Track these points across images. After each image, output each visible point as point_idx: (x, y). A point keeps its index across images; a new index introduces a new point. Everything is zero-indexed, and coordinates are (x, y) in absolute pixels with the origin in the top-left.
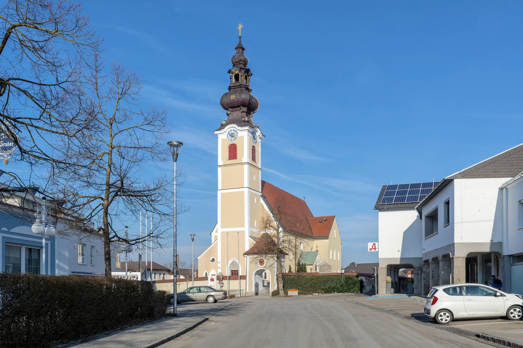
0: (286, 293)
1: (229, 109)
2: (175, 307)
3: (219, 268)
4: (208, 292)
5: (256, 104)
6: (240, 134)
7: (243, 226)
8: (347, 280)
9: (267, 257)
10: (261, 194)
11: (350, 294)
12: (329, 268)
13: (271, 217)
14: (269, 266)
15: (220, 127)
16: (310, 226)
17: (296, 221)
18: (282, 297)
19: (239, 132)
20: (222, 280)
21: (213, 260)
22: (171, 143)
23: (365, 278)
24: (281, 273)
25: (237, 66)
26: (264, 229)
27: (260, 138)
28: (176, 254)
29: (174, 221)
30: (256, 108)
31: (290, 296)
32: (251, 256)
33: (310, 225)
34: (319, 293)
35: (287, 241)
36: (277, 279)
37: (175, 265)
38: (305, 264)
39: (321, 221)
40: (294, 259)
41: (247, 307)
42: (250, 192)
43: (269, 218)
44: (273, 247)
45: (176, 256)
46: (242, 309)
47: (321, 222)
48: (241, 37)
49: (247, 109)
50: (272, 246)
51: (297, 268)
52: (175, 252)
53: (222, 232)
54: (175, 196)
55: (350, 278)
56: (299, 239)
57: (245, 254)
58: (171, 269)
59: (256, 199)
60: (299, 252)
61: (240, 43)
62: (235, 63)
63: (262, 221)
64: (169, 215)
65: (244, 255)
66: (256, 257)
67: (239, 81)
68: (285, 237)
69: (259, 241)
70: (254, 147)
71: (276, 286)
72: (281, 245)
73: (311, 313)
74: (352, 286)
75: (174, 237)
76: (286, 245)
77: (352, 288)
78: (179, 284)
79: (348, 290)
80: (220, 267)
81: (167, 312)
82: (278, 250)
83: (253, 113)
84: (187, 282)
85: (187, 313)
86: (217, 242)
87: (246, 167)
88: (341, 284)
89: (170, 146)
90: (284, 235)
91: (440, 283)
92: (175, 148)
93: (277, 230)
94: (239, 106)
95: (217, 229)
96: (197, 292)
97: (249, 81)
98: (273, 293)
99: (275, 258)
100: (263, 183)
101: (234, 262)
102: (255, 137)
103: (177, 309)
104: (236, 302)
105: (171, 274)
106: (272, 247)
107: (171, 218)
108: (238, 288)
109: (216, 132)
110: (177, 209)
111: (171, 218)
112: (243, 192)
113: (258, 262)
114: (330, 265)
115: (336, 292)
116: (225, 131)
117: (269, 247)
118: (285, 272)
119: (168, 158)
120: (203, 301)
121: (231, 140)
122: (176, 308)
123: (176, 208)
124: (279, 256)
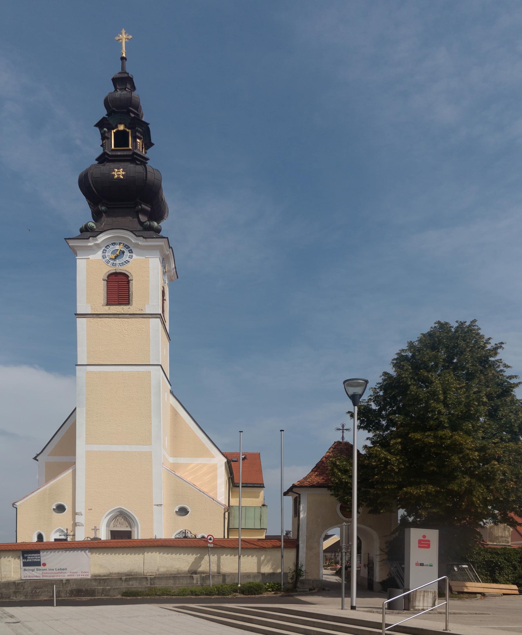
67: (128, 146)
91: (362, 526)
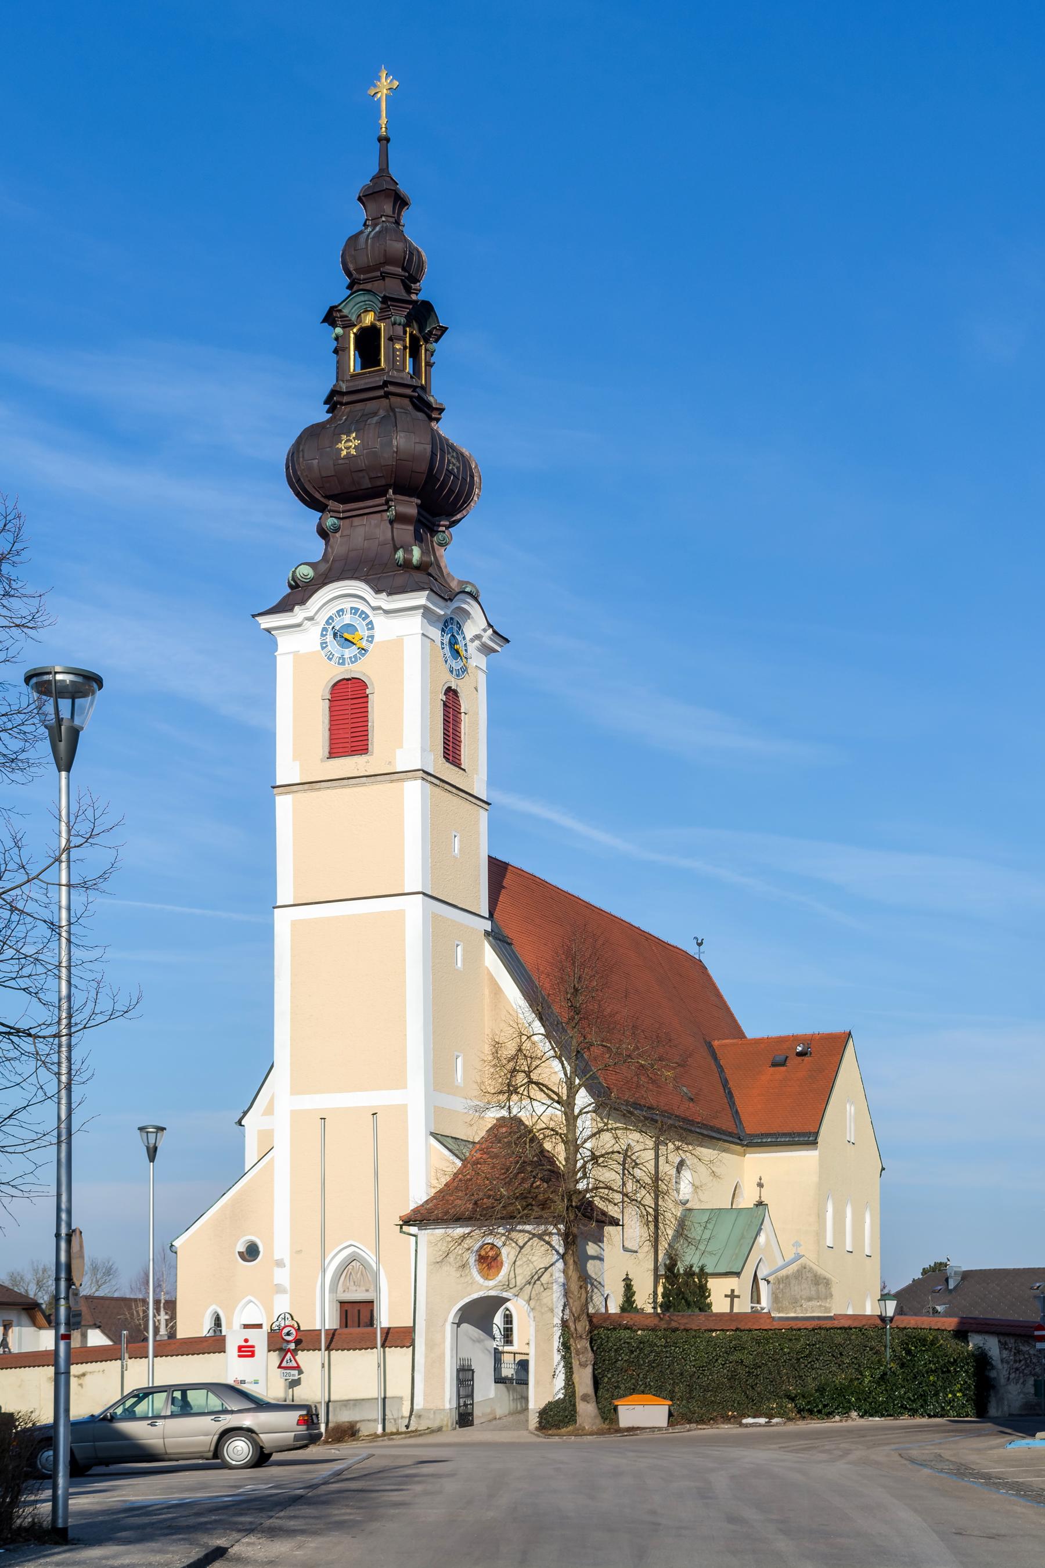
0: (609, 1414)
1: (332, 504)
2: (60, 1492)
3: (279, 1289)
4: (225, 1411)
5: (464, 479)
6: (385, 628)
7: (399, 1082)
8: (909, 1352)
9: (514, 1235)
10: (488, 925)
11: (925, 1420)
12: (821, 1288)
13: (535, 1038)
14: (524, 1281)
15: (289, 595)
16: (725, 1083)
17: (661, 1059)
18: (591, 1434)
19: (379, 620)
20: (294, 1352)
21: (251, 1252)
22: (46, 677)
23: (999, 1341)
24: (585, 1316)
25: (368, 286)
26: (503, 1098)
27: (486, 650)
28: (69, 1224)
29: (59, 1064)
30: (464, 502)
31: (631, 1430)
32: (439, 1232)
33: (726, 1080)
34: (770, 1417)
35: (615, 1156)
36: (566, 1346)
37: (63, 1284)
38: (702, 1269)
39: (780, 1058)
40: (647, 1247)
41: (418, 1488)
42: (435, 917)
43: (527, 1045)
44: (545, 1185)
45: (69, 1237)
46: (395, 1497)
47: (783, 1064)
48: (388, 140)
49: (418, 506)
50: (542, 1180)
51: (660, 1290)
52: (64, 1216)
53: (296, 1116)
54: (64, 941)
55: (923, 1341)
56: (671, 1146)
57: (407, 1222)
58: (44, 1299)
59: (464, 950)
60: (671, 1212)
61: (383, 172)
62: (359, 270)
63: (490, 1058)
64: (36, 1037)
65: (405, 1228)
66: (464, 1237)
67: (379, 365)
68: (606, 1136)
69: (478, 1155)
70: (455, 692)
71: (560, 1382)
72: (585, 1176)
73: (732, 1519)
74: (934, 1384)
75: (59, 1143)
76: (610, 1175)
77: (936, 1394)
78: (84, 1375)
79: (914, 1401)
80: (287, 1284)
81: (19, 1521)
82: (570, 1200)
83: (448, 527)
84: (119, 1362)
85: (118, 1520)
86: (272, 1159)
87: (414, 790)
88: (878, 1374)
89: (40, 692)
90: (601, 1125)
92: (65, 704)
93: (567, 1104)
94: (378, 492)
95: (273, 1095)
96: (173, 1416)
97: (429, 365)
98: (543, 1413)
99: (557, 1241)
100: (498, 870)
101: (353, 1259)
102: (460, 647)
103: (70, 1502)
104: (368, 1463)
105: (44, 1322)
106: (538, 1187)
107: (47, 1050)
108: (372, 1391)
109: (266, 622)
110: (76, 1004)
111: (47, 1050)
112: (401, 914)
113: (472, 1259)
114: (828, 1276)
115: (854, 1414)
116: (311, 614)
117: (526, 1185)
118: (603, 1310)
119: (30, 754)
120: (202, 1458)
121: (342, 657)
122: (68, 1496)
123: (69, 997)
124: (575, 1230)
